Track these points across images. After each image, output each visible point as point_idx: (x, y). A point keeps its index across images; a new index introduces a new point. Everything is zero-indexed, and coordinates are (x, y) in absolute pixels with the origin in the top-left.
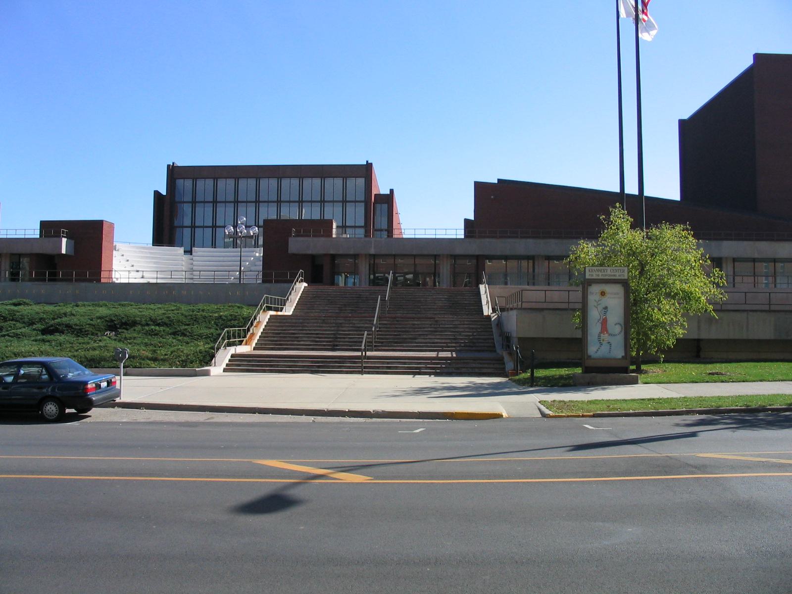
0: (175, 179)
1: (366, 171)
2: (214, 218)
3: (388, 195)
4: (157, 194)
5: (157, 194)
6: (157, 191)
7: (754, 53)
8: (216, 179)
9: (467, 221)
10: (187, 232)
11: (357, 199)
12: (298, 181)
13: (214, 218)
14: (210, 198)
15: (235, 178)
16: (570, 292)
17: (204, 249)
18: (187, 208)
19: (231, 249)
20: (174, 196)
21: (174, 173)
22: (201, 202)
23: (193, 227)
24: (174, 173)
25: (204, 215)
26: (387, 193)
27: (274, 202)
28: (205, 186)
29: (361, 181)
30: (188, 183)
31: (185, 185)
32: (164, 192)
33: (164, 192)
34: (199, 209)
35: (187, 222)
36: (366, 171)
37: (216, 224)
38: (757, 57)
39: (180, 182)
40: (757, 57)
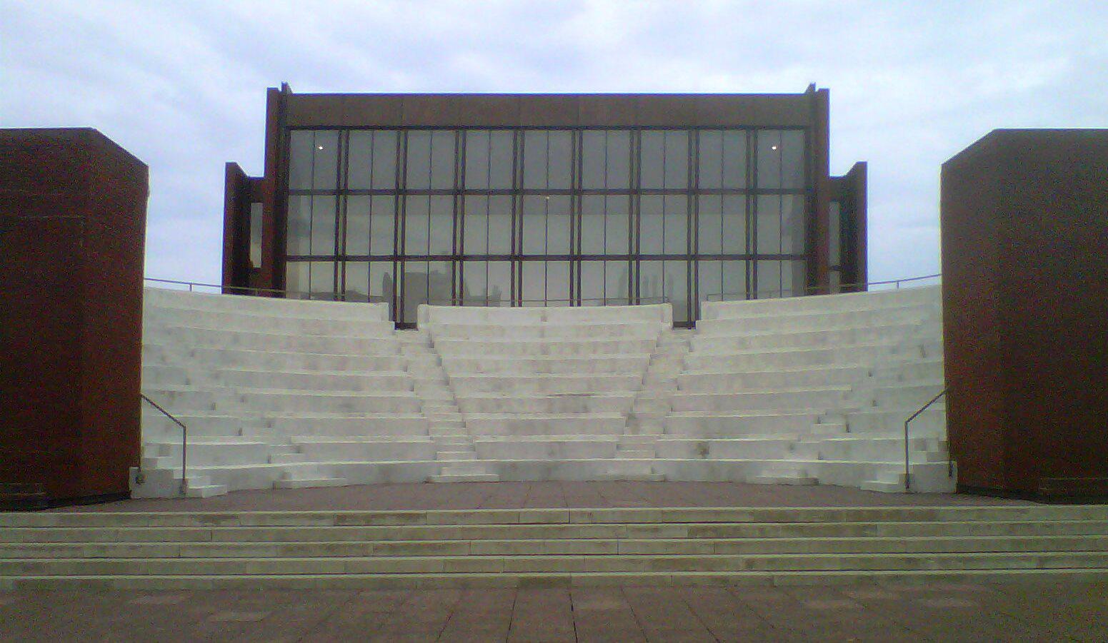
1: (809, 113)
3: (260, 178)
4: (234, 175)
5: (234, 175)
11: (317, 187)
12: (395, 138)
14: (737, 180)
17: (723, 302)
19: (506, 310)
20: (286, 175)
21: (287, 114)
22: (439, 192)
24: (287, 114)
25: (371, 227)
26: (260, 176)
27: (708, 192)
28: (373, 157)
29: (795, 140)
30: (324, 144)
31: (314, 150)
32: (255, 168)
33: (255, 168)
34: (357, 217)
36: (809, 113)
37: (344, 250)
39: (300, 140)
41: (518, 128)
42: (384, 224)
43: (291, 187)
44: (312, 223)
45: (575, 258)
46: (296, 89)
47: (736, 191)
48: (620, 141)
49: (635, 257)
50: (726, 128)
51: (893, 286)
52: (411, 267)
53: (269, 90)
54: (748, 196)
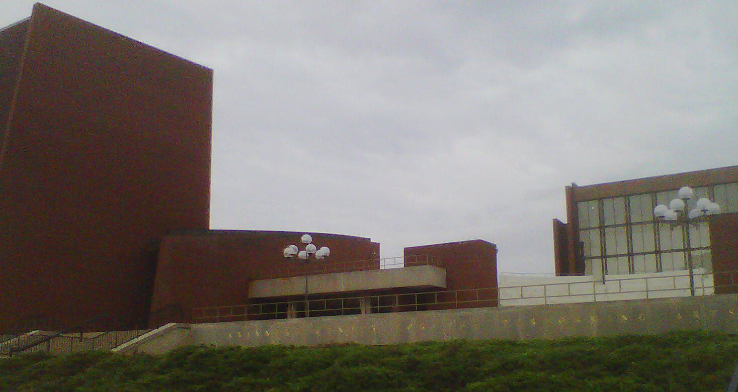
0: (576, 203)
2: (657, 240)
4: (557, 223)
5: (557, 223)
6: (557, 219)
7: (36, 2)
8: (601, 199)
9: (557, 224)
10: (597, 263)
13: (657, 240)
15: (625, 196)
16: (648, 280)
18: (595, 236)
21: (575, 196)
23: (604, 256)
28: (614, 210)
30: (594, 206)
31: (589, 212)
32: (564, 220)
33: (564, 220)
34: (636, 236)
35: (597, 252)
38: (39, 9)
39: (582, 206)
40: (39, 9)
41: (627, 196)
42: (623, 239)
43: (580, 228)
44: (591, 241)
45: (658, 252)
46: (580, 184)
47: (621, 225)
48: (620, 202)
49: (658, 252)
50: (590, 200)
51: (543, 276)
52: (693, 253)
53: (566, 187)
54: (655, 225)
